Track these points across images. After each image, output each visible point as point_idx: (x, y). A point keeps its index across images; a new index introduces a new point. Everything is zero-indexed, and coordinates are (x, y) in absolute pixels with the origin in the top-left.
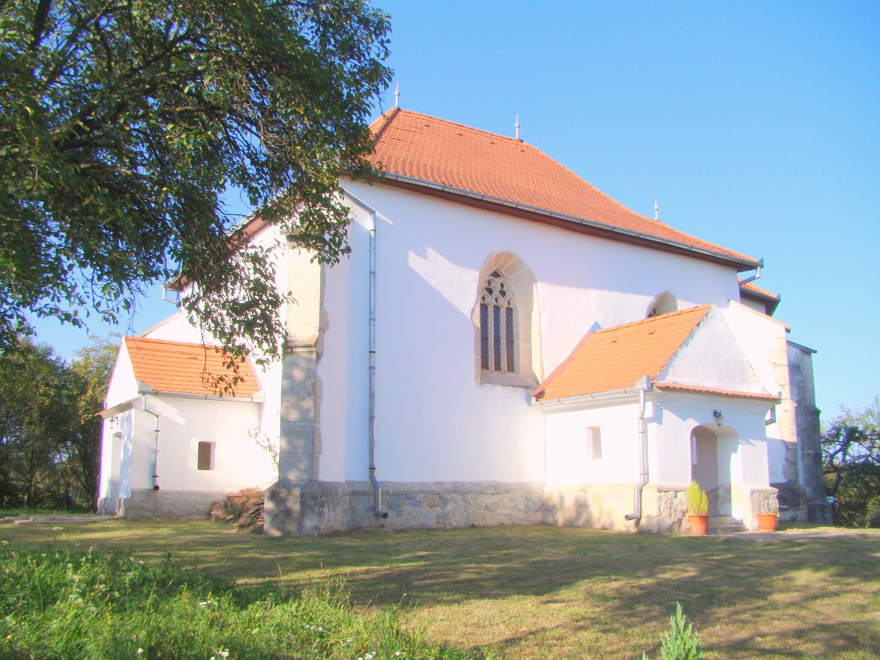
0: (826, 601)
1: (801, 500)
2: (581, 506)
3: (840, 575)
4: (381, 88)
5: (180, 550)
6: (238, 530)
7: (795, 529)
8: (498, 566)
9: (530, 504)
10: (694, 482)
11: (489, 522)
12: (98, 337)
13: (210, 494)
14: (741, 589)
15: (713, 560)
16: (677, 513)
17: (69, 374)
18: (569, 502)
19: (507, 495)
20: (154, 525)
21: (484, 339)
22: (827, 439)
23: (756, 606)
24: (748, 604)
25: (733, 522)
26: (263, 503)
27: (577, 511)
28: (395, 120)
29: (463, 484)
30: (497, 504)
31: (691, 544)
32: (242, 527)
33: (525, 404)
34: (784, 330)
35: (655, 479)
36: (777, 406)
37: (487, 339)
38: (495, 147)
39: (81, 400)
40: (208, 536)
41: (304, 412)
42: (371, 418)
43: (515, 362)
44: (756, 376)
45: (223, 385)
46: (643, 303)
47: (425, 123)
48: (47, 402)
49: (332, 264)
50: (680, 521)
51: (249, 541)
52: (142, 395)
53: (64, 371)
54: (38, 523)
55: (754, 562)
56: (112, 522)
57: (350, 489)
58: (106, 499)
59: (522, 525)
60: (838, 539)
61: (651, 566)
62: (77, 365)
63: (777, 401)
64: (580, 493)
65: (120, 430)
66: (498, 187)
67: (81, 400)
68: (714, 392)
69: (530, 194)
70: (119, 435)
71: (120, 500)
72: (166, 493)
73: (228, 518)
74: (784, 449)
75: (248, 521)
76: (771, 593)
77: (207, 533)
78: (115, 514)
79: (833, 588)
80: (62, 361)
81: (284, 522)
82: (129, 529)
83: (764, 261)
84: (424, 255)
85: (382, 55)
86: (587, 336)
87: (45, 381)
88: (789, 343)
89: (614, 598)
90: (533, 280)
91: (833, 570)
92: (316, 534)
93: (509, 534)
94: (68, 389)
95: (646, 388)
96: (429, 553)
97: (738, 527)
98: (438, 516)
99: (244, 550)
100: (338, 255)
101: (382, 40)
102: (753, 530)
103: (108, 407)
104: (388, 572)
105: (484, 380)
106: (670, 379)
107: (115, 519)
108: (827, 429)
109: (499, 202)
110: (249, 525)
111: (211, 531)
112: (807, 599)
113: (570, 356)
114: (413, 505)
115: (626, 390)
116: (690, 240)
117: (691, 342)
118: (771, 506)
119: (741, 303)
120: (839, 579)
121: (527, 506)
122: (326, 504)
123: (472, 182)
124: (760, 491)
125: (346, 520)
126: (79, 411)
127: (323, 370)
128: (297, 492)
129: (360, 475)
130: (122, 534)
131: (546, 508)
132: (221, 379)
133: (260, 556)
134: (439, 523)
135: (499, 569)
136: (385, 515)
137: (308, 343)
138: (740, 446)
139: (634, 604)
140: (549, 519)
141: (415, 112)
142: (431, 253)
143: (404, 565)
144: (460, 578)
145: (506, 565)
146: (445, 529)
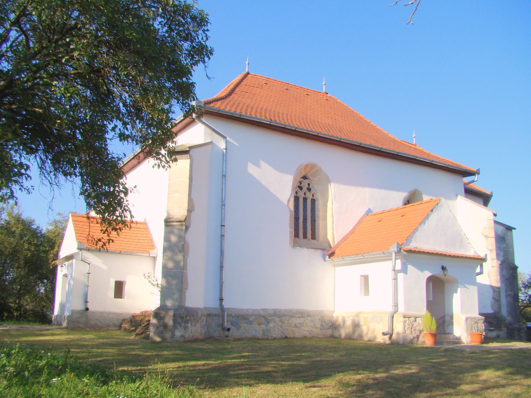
0: (495, 390)
1: (502, 324)
2: (356, 326)
3: (511, 373)
4: (206, 59)
5: (92, 348)
6: (135, 337)
7: (495, 343)
8: (289, 363)
9: (324, 324)
10: (428, 312)
11: (297, 335)
12: (62, 214)
13: (121, 314)
14: (441, 381)
15: (431, 362)
16: (416, 331)
17: (44, 237)
18: (349, 323)
19: (309, 318)
20: (85, 333)
21: (296, 218)
22: (527, 285)
23: (445, 392)
24: (441, 391)
25: (454, 338)
26: (150, 321)
27: (353, 329)
28: (245, 80)
29: (280, 311)
30: (302, 323)
31: (425, 351)
32: (137, 335)
33: (321, 259)
34: (492, 214)
35: (402, 309)
36: (484, 263)
37: (298, 218)
38: (309, 97)
39: (51, 253)
40: (114, 340)
41: (177, 263)
42: (222, 267)
43: (316, 233)
44: (470, 244)
45: (101, 244)
46: (401, 196)
47: (264, 82)
48: (29, 255)
49: (166, 169)
50: (418, 337)
51: (138, 344)
52: (79, 250)
53: (41, 235)
54: (12, 330)
55: (458, 364)
56: (58, 330)
57: (206, 312)
58: (57, 316)
59: (318, 338)
60: (521, 350)
61: (388, 366)
62: (49, 231)
63: (484, 260)
64: (356, 317)
65: (66, 272)
66: (308, 123)
67: (51, 253)
68: (428, 253)
69: (329, 127)
70: (65, 276)
71: (65, 316)
72: (93, 313)
73: (131, 329)
74: (492, 291)
75: (142, 331)
76: (460, 385)
77: (114, 338)
78: (62, 325)
79: (503, 382)
80: (40, 229)
81: (162, 333)
82: (67, 334)
83: (480, 170)
84: (258, 165)
85: (205, 38)
86: (363, 218)
87: (29, 241)
88: (495, 222)
89: (354, 386)
90: (329, 181)
91: (508, 370)
92: (182, 340)
93: (307, 343)
94: (43, 246)
95: (396, 251)
96: (250, 354)
97: (458, 341)
98: (263, 331)
99: (133, 349)
100: (169, 163)
101: (204, 29)
102: (467, 343)
103: (61, 257)
104: (217, 365)
105: (295, 244)
106: (412, 246)
107: (61, 328)
108: (527, 279)
109: (307, 132)
110: (142, 333)
111: (118, 337)
112: (482, 389)
113: (352, 230)
114: (247, 323)
115: (384, 252)
116: (432, 156)
117: (427, 222)
118: (479, 328)
119: (466, 197)
120: (509, 376)
121: (322, 325)
122: (190, 322)
123: (291, 120)
124: (472, 318)
125: (203, 332)
126: (49, 260)
127: (190, 237)
128: (171, 313)
129: (214, 304)
130: (61, 337)
131: (334, 326)
132: (100, 240)
133: (142, 353)
134: (264, 335)
135: (289, 365)
136: (229, 330)
137: (180, 219)
138: (459, 289)
139: (365, 389)
140: (336, 334)
141: (258, 75)
142: (263, 164)
143: (230, 361)
144: (260, 370)
145: (295, 362)
146: (268, 339)
